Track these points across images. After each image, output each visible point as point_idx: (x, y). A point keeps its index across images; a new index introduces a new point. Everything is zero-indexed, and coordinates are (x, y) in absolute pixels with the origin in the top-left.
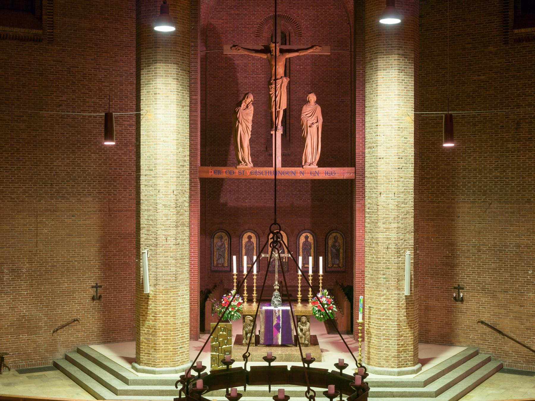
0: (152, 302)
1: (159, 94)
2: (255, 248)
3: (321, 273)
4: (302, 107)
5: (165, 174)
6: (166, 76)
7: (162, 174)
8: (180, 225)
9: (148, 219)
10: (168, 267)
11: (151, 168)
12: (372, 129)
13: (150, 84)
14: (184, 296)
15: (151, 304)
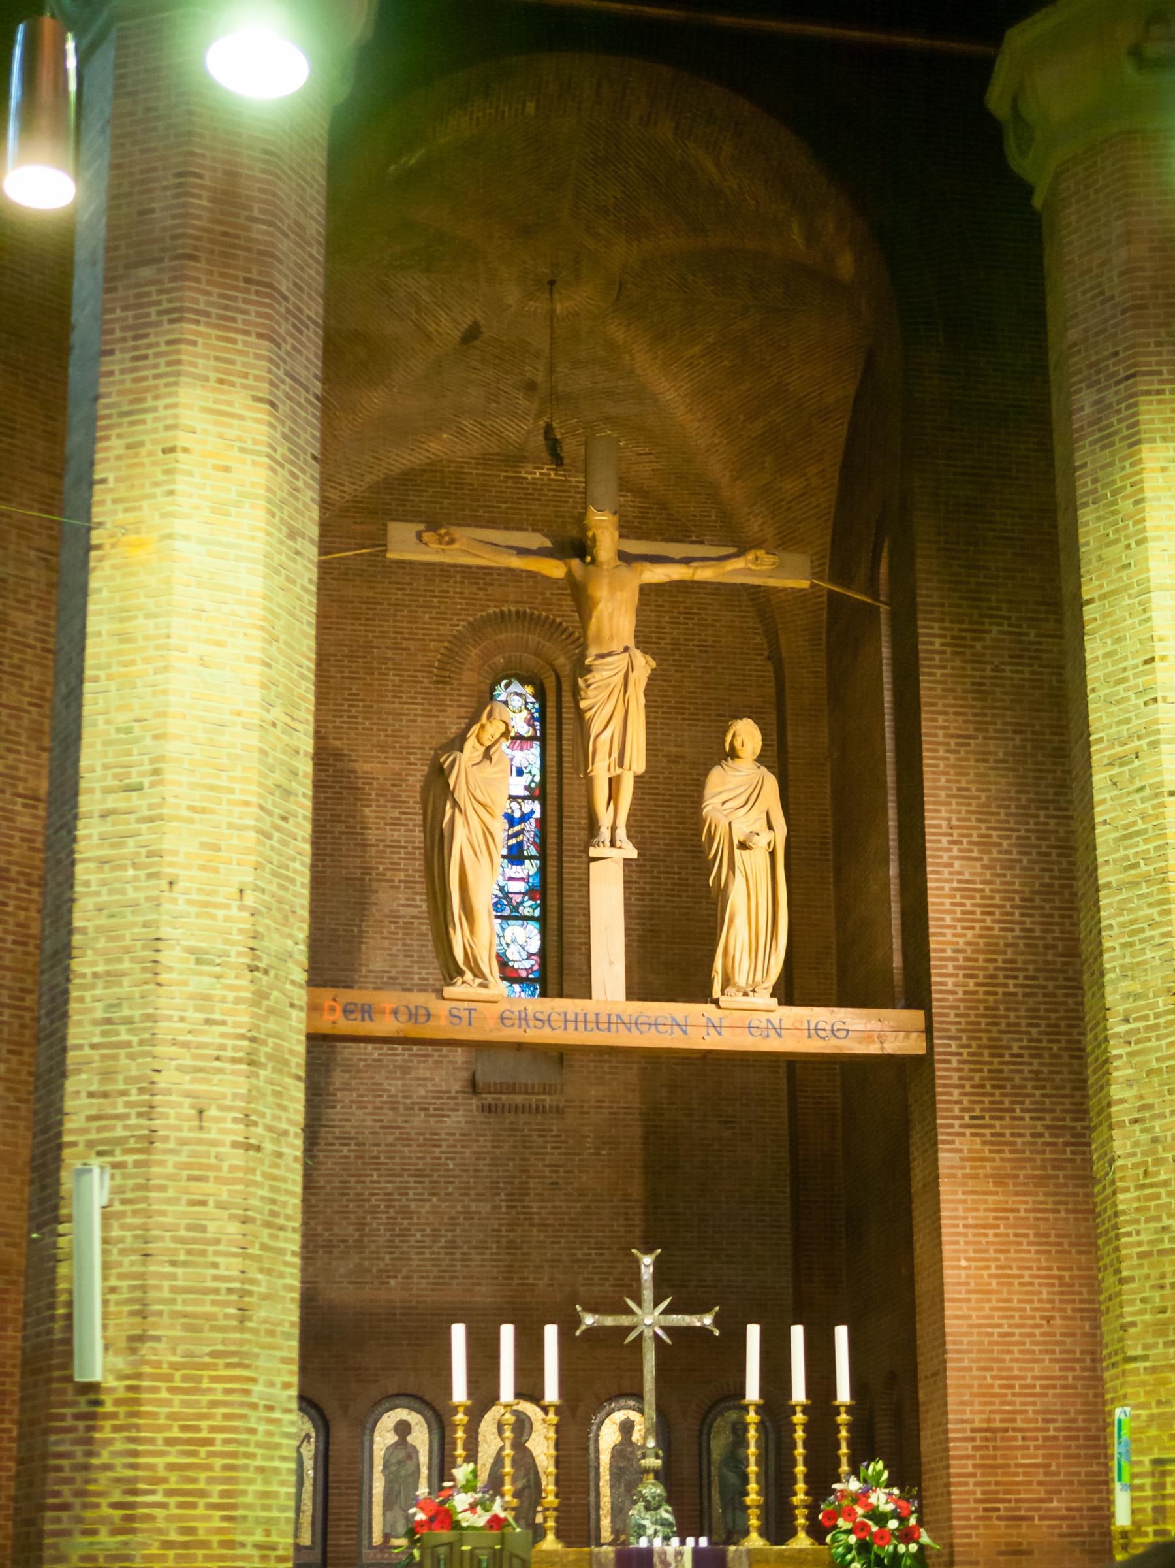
0: (116, 1429)
1: (185, 450)
2: (424, 1471)
3: (844, 1395)
4: (706, 775)
5: (204, 811)
6: (221, 381)
7: (192, 809)
8: (269, 1056)
9: (109, 1021)
10: (203, 1253)
11: (134, 780)
12: (1123, 680)
13: (145, 411)
14: (276, 1415)
15: (109, 1442)
